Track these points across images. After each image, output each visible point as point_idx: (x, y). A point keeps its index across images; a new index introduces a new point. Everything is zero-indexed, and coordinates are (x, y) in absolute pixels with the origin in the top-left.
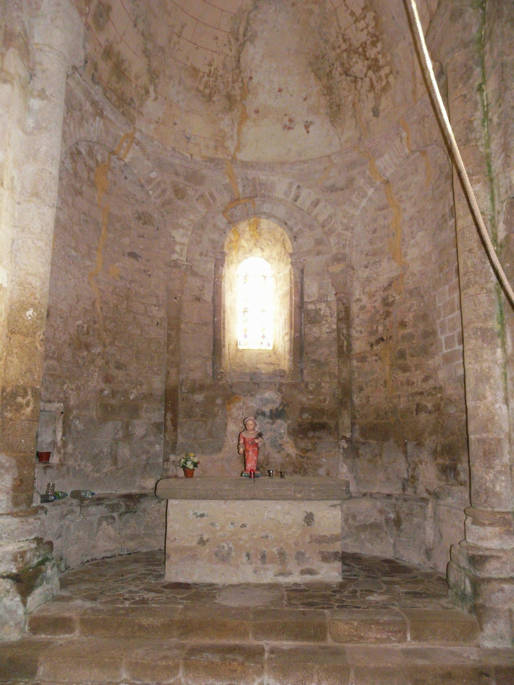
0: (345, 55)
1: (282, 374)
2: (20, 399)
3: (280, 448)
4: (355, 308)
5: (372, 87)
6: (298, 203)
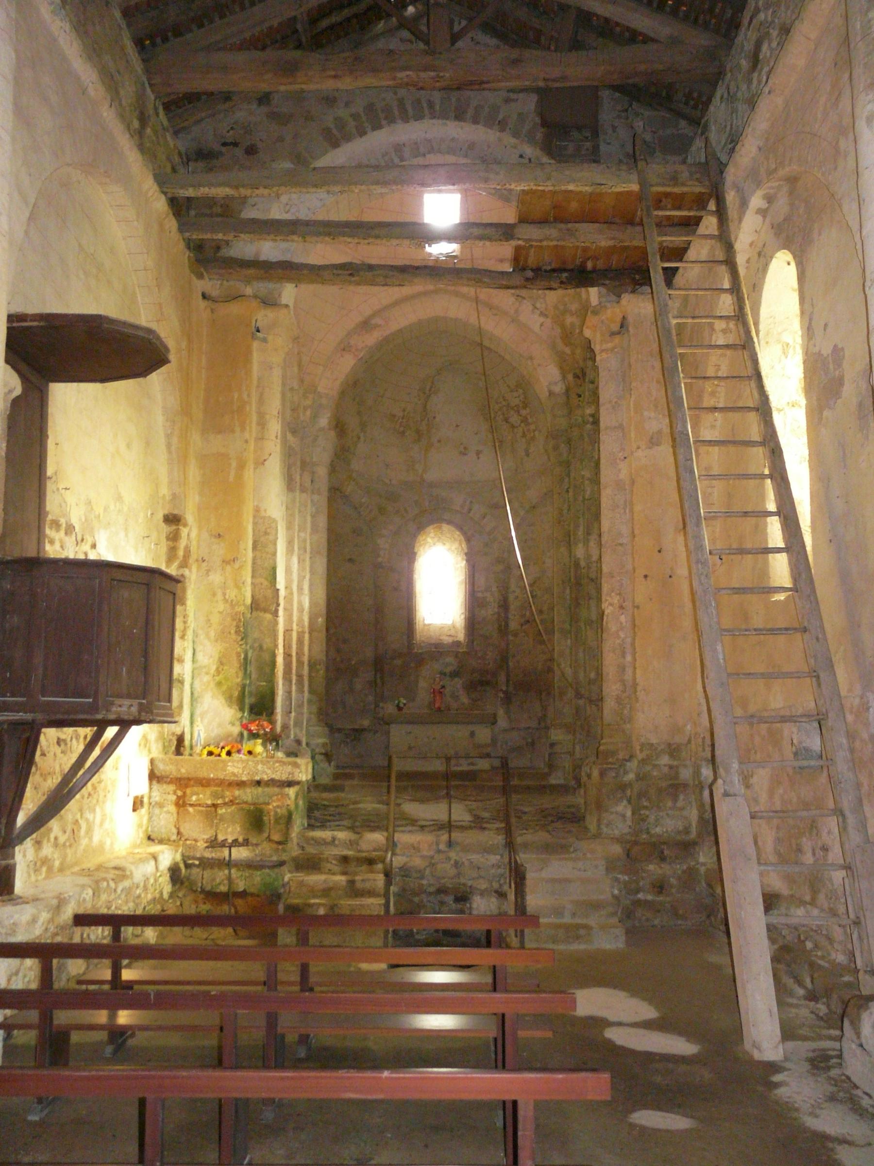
0: (505, 408)
1: (457, 644)
2: (318, 667)
3: (456, 698)
4: (511, 598)
5: (524, 435)
6: (471, 515)
